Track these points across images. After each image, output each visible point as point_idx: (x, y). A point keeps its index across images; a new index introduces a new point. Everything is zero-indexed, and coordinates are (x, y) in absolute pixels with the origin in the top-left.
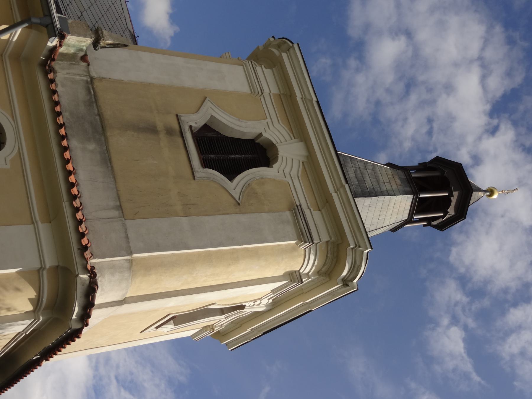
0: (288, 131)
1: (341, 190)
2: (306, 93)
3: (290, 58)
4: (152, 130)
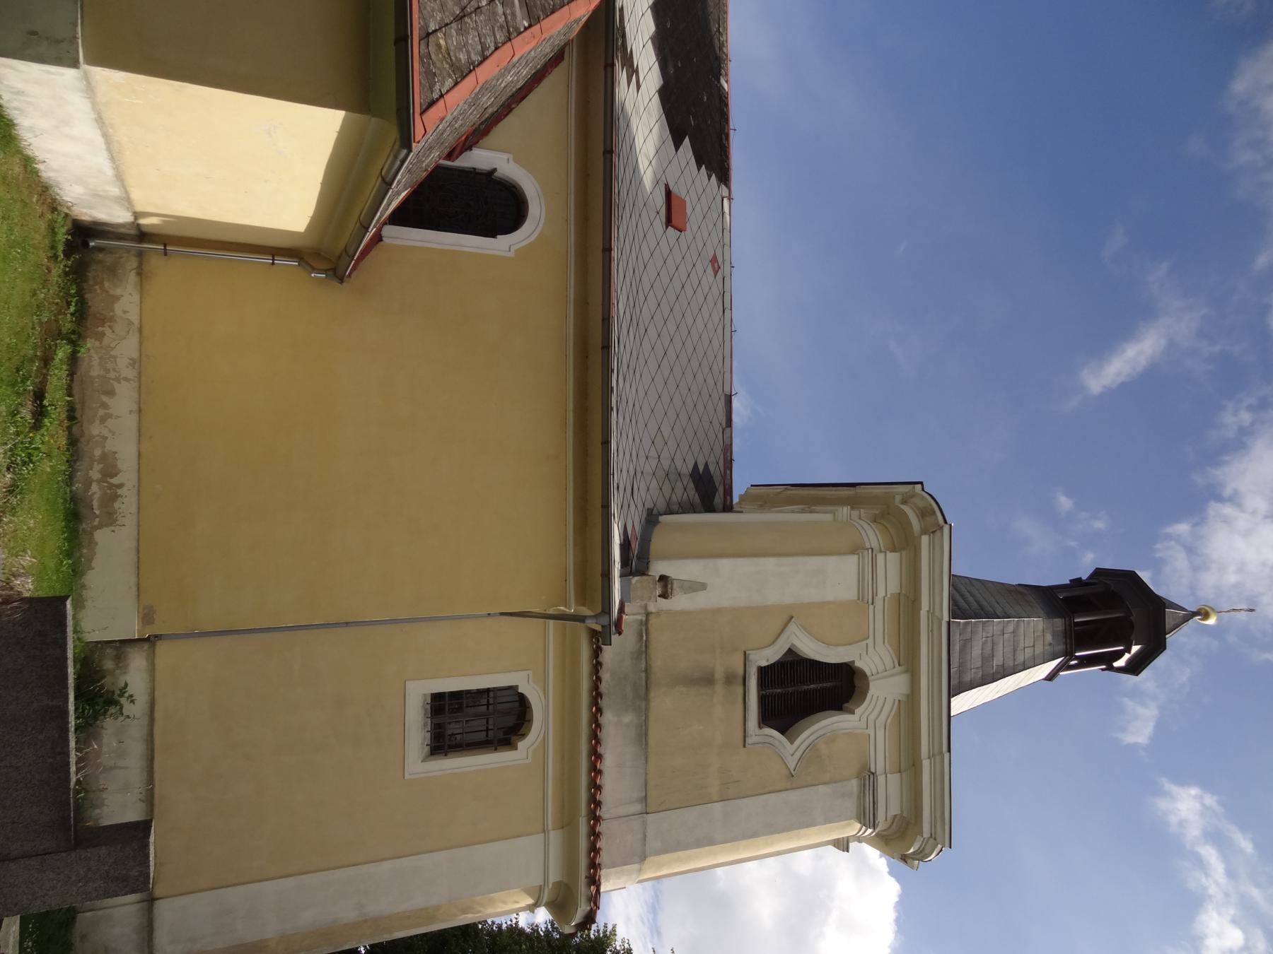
0: (893, 655)
1: (938, 758)
2: (937, 607)
3: (932, 545)
4: (707, 680)
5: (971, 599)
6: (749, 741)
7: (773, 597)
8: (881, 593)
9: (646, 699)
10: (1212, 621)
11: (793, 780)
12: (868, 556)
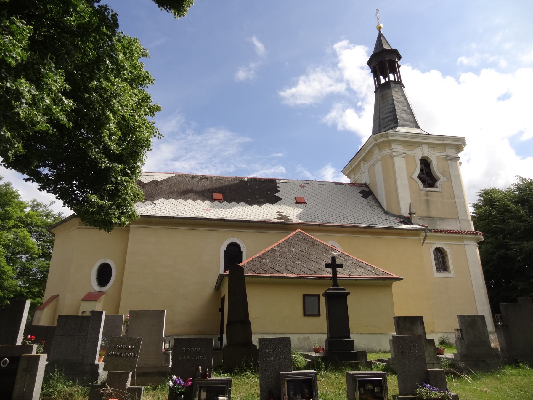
2: (407, 136)
4: (427, 201)
5: (388, 115)
6: (441, 191)
7: (406, 182)
8: (402, 151)
9: (433, 218)
10: (381, 25)
11: (449, 179)
12: (394, 154)
